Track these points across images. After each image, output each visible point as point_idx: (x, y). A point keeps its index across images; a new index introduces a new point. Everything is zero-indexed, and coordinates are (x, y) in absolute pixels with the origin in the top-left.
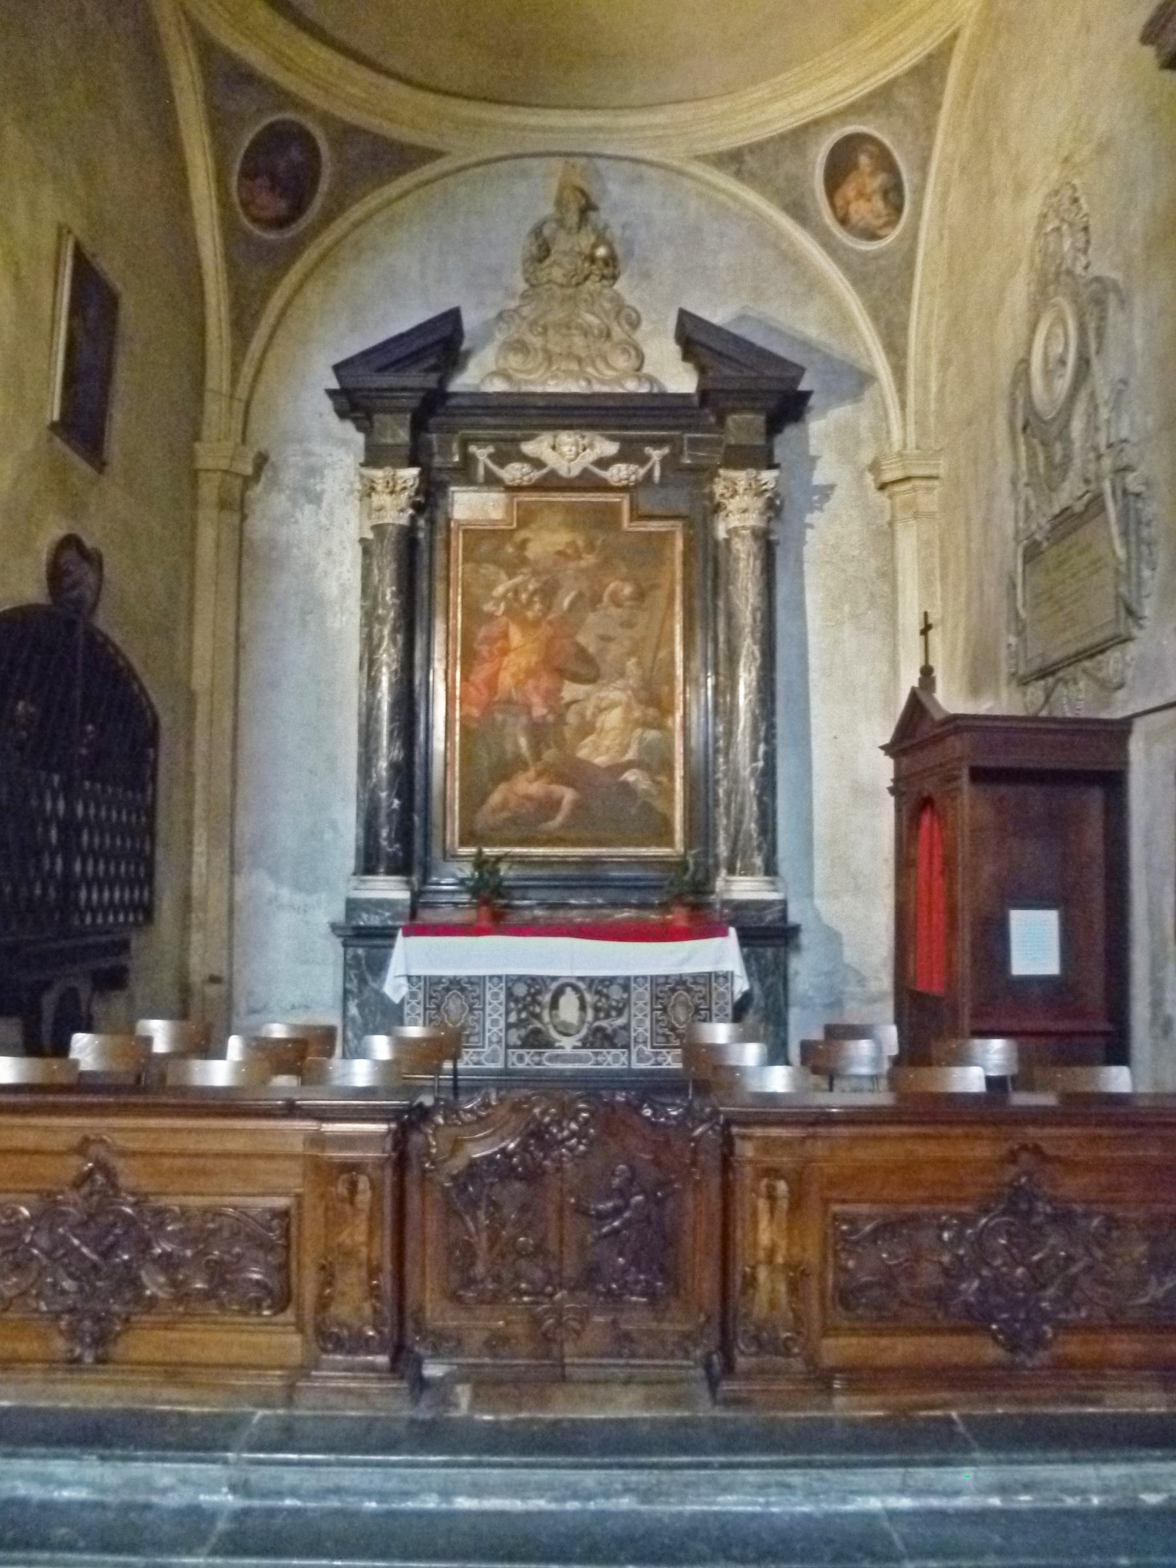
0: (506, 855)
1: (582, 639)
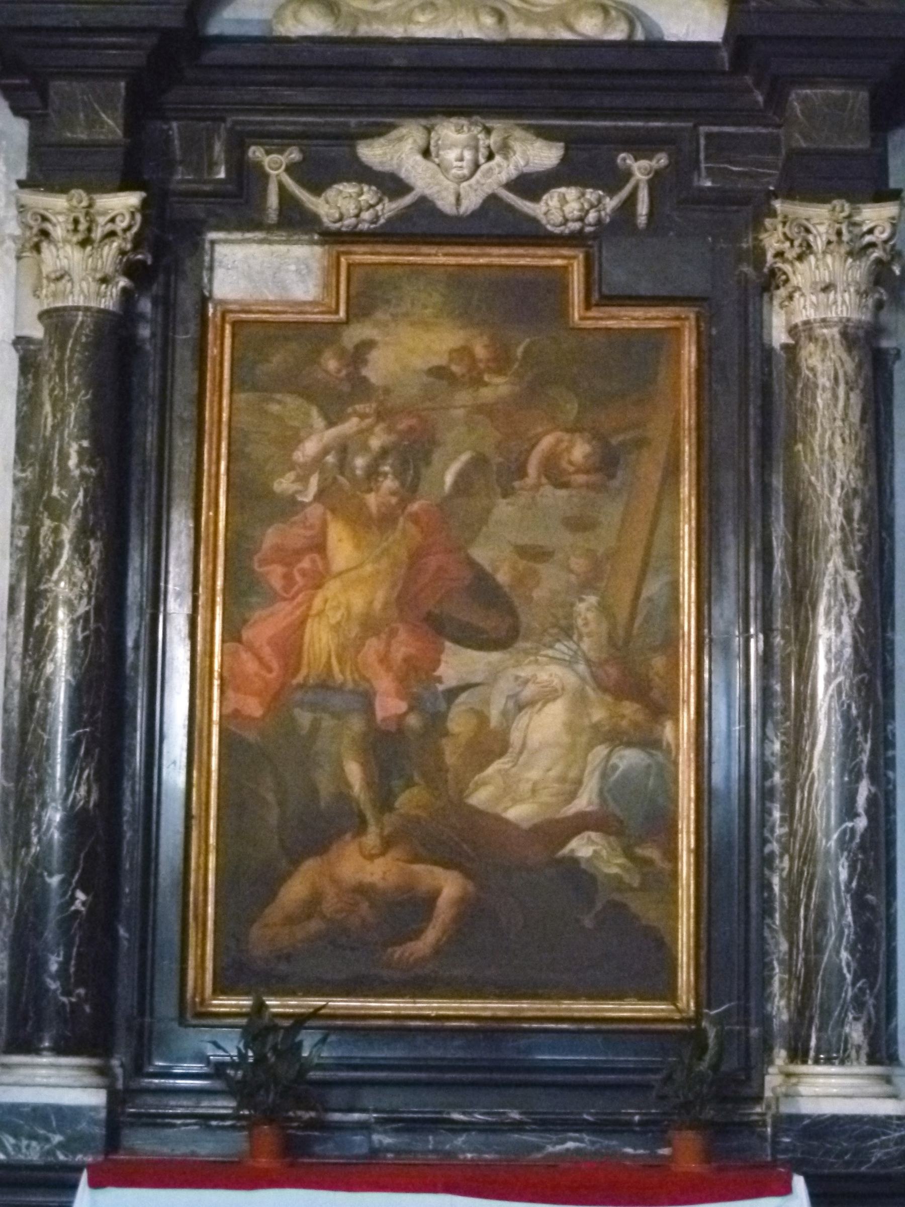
0: (316, 1014)
1: (481, 554)
